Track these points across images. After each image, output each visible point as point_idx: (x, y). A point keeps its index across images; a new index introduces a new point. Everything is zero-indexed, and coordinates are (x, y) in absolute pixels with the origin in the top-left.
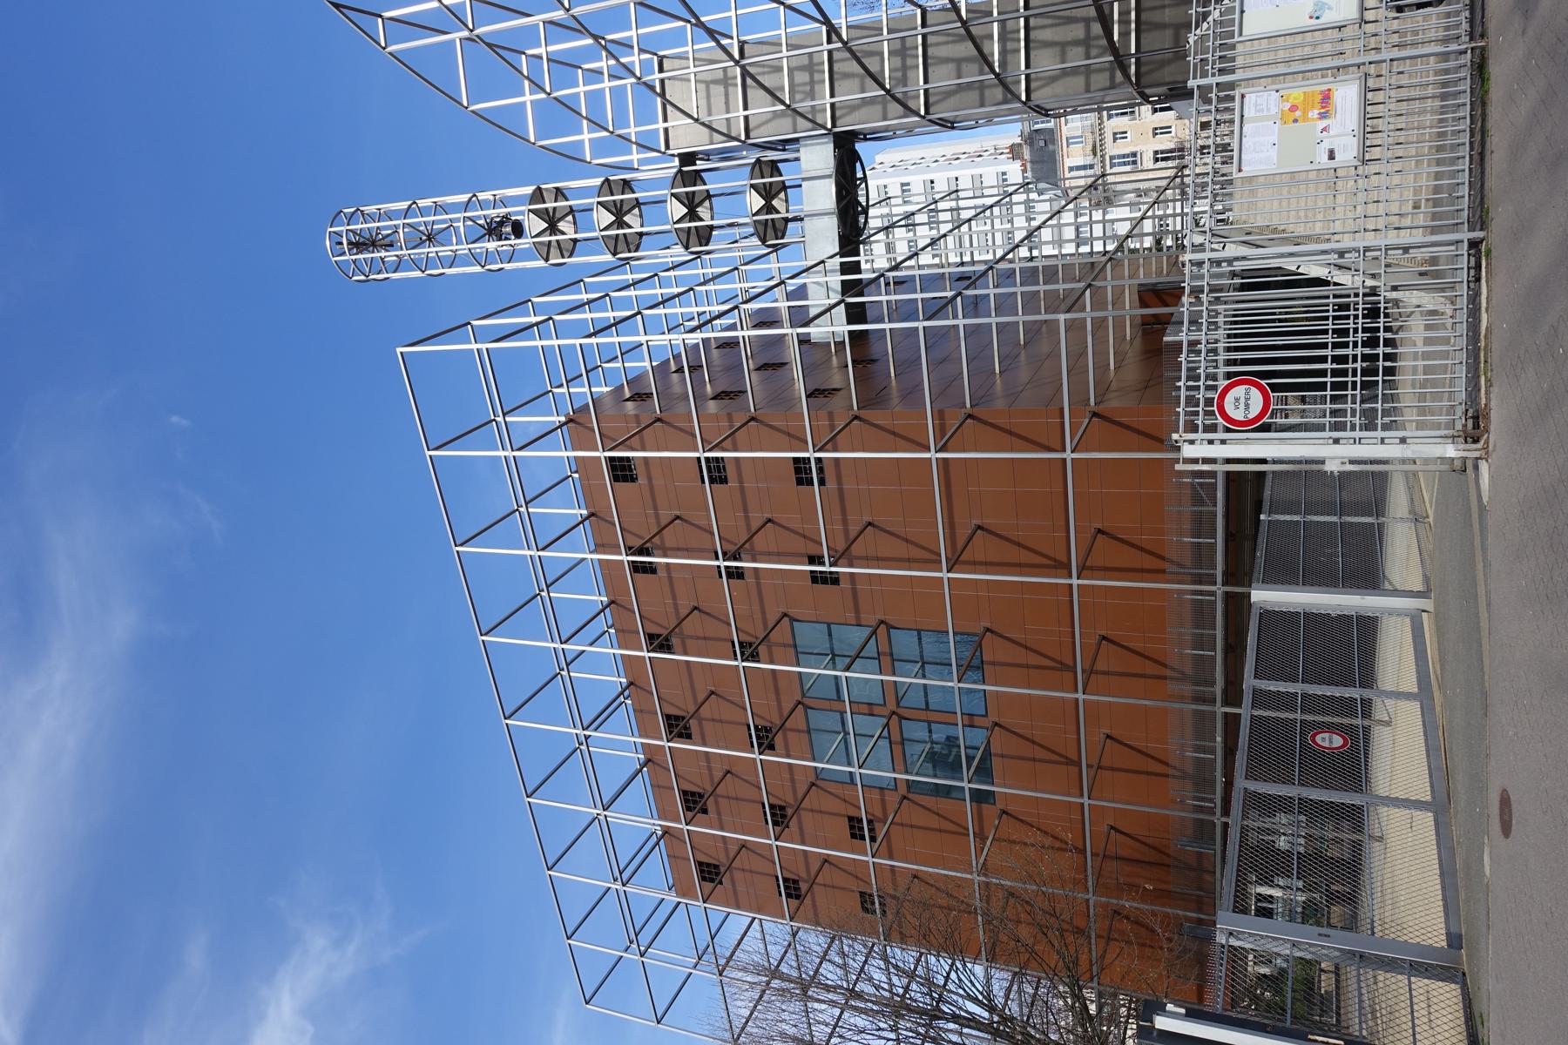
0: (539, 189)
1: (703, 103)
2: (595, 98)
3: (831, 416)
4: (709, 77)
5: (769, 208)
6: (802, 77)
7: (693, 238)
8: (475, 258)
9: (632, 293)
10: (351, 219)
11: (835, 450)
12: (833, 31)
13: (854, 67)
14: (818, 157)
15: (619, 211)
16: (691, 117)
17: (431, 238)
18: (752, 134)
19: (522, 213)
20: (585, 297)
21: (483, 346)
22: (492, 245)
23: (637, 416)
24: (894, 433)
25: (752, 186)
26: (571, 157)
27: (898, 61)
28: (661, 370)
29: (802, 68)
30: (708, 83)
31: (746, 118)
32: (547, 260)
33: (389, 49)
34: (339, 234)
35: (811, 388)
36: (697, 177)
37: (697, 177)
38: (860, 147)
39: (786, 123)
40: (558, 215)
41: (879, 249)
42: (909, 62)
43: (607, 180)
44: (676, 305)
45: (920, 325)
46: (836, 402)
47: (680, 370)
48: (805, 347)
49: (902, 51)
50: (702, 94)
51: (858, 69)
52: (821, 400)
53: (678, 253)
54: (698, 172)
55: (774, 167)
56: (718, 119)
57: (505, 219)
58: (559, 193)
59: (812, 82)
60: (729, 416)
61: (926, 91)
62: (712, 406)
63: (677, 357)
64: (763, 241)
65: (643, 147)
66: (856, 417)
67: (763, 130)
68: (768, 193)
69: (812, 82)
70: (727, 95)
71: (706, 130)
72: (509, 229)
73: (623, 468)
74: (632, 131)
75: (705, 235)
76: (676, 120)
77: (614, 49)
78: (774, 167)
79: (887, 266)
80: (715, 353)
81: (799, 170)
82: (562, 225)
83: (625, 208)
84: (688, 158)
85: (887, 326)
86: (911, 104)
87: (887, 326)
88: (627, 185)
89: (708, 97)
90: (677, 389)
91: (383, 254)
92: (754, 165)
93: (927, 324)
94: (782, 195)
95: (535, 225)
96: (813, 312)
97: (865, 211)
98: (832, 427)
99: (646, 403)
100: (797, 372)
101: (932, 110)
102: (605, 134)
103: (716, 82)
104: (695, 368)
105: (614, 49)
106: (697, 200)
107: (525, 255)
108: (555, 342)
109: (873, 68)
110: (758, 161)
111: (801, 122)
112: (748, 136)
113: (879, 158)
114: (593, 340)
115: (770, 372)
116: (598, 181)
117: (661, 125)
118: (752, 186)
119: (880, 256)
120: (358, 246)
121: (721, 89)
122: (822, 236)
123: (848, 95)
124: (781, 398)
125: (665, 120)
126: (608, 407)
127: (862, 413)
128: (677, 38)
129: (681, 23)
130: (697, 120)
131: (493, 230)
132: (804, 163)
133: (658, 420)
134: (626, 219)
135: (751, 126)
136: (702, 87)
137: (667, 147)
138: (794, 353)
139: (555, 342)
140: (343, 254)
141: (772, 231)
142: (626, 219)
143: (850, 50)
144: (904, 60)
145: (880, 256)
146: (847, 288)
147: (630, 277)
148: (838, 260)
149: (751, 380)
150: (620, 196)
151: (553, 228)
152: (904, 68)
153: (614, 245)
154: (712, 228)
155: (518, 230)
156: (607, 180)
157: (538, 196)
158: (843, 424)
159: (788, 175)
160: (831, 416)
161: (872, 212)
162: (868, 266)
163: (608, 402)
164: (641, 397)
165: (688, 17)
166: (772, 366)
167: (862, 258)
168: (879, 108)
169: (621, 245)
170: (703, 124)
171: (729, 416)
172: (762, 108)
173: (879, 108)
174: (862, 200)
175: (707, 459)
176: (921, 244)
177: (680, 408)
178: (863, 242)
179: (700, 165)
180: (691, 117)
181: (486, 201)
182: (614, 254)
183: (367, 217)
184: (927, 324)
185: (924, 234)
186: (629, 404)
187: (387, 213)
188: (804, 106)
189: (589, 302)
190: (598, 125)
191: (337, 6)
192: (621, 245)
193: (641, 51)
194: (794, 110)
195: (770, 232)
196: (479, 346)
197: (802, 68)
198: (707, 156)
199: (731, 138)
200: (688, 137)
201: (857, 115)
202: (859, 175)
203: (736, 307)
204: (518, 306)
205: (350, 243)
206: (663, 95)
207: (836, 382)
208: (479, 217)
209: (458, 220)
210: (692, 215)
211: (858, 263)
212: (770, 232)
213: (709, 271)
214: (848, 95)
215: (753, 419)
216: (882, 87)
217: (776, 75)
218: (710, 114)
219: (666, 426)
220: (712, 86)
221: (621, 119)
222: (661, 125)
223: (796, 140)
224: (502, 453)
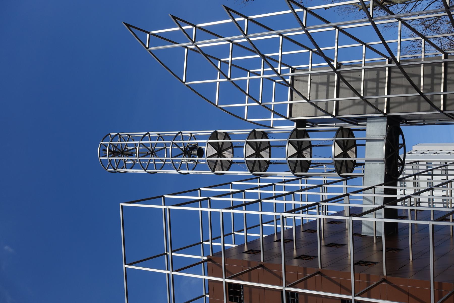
0: (216, 132)
1: (313, 94)
2: (253, 83)
3: (368, 277)
4: (319, 81)
5: (344, 154)
6: (371, 85)
7: (298, 167)
8: (175, 167)
9: (258, 191)
10: (113, 138)
11: (369, 297)
12: (393, 59)
13: (405, 81)
14: (377, 129)
15: (258, 149)
16: (305, 99)
17: (153, 153)
18: (340, 113)
19: (204, 144)
20: (231, 190)
21: (168, 207)
22: (185, 159)
23: (249, 262)
24: (408, 294)
25: (336, 141)
26: (236, 117)
27: (429, 81)
28: (269, 240)
29: (372, 80)
30: (317, 84)
31: (337, 102)
32: (213, 171)
33: (150, 49)
34: (105, 146)
35: (358, 260)
36: (305, 134)
37: (305, 134)
38: (404, 128)
39: (360, 108)
40: (224, 147)
41: (409, 184)
42: (436, 81)
43: (254, 131)
44: (284, 203)
45: (431, 223)
46: (373, 270)
47: (279, 241)
48: (357, 238)
49: (432, 76)
50: (314, 89)
51: (407, 83)
52: (363, 267)
53: (290, 175)
54: (306, 132)
55: (350, 133)
56: (321, 101)
57: (194, 147)
58: (227, 136)
59: (377, 88)
60: (305, 269)
61: (445, 96)
62: (295, 262)
63: (278, 234)
64: (339, 173)
65: (277, 114)
66: (384, 280)
67: (346, 111)
68: (345, 146)
69: (377, 88)
70: (328, 91)
71: (313, 108)
72: (195, 152)
73: (236, 293)
74: (273, 104)
75: (305, 166)
76: (298, 101)
77: (270, 62)
78: (350, 133)
79: (413, 192)
80: (302, 234)
81: (365, 135)
82: (225, 153)
83: (262, 147)
84: (301, 123)
85: (409, 222)
86: (435, 104)
87: (409, 222)
88: (265, 135)
89: (317, 91)
90: (276, 250)
91: (126, 158)
92: (338, 131)
93: (435, 223)
94: (353, 149)
95: (210, 151)
96: (364, 211)
97: (403, 164)
98: (368, 284)
99: (256, 258)
100: (350, 251)
101: (448, 108)
102: (257, 104)
103: (322, 84)
104: (288, 241)
105: (270, 62)
106: (303, 147)
107: (203, 168)
108: (209, 210)
109: (416, 83)
110: (341, 128)
111: (369, 108)
112: (337, 113)
113: (414, 148)
114: (232, 211)
115: (333, 248)
116: (248, 131)
117: (289, 102)
118: (336, 141)
119: (410, 188)
120: (113, 153)
121: (325, 88)
122: (375, 174)
123: (398, 95)
124: (339, 262)
125: (291, 99)
126: (234, 255)
127: (389, 278)
128: (303, 59)
129: (307, 51)
130: (308, 101)
131: (187, 151)
132: (368, 132)
133: (261, 266)
134: (262, 153)
135: (340, 108)
136: (314, 86)
137: (290, 115)
138: (349, 227)
139: (209, 210)
140: (106, 156)
141: (345, 169)
142: (262, 153)
143: (401, 68)
144: (432, 80)
145: (410, 188)
146: (387, 201)
147: (258, 184)
148: (384, 187)
149: (321, 251)
150: (261, 141)
151: (220, 154)
152: (432, 84)
153: (252, 166)
154: (309, 163)
155: (201, 153)
156: (254, 131)
157: (215, 135)
158: (375, 283)
159: (358, 137)
160: (368, 277)
161: (406, 167)
162: (402, 192)
163: (234, 252)
164: (253, 251)
165: (311, 45)
166: (335, 245)
167: (398, 187)
168: (416, 105)
169: (256, 167)
170: (312, 103)
171: (305, 269)
172: (347, 97)
173: (416, 105)
174: (401, 156)
175: (287, 292)
176: (435, 184)
177: (276, 261)
178: (401, 180)
179: (307, 128)
180: (305, 99)
181: (186, 136)
182: (252, 171)
183: (122, 138)
184: (435, 223)
185: (437, 180)
186: (246, 255)
187: (133, 138)
188: (371, 98)
189: (233, 193)
190: (253, 99)
191: (128, 25)
192: (256, 167)
193: (282, 64)
194: (366, 100)
195: (344, 168)
196: (165, 207)
197: (372, 80)
198: (313, 123)
199: (327, 114)
200: (303, 111)
201: (402, 108)
202: (401, 142)
203: (317, 204)
204: (193, 191)
205: (110, 151)
206: (292, 85)
207: (375, 258)
208: (181, 143)
209: (168, 145)
210: (299, 154)
211: (396, 190)
212: (344, 168)
213: (305, 185)
214: (398, 95)
215: (319, 273)
216: (419, 91)
217: (357, 83)
218: (317, 98)
219: (268, 271)
220: (320, 86)
221: (267, 96)
222: (289, 102)
223: (364, 119)
224: (167, 272)
